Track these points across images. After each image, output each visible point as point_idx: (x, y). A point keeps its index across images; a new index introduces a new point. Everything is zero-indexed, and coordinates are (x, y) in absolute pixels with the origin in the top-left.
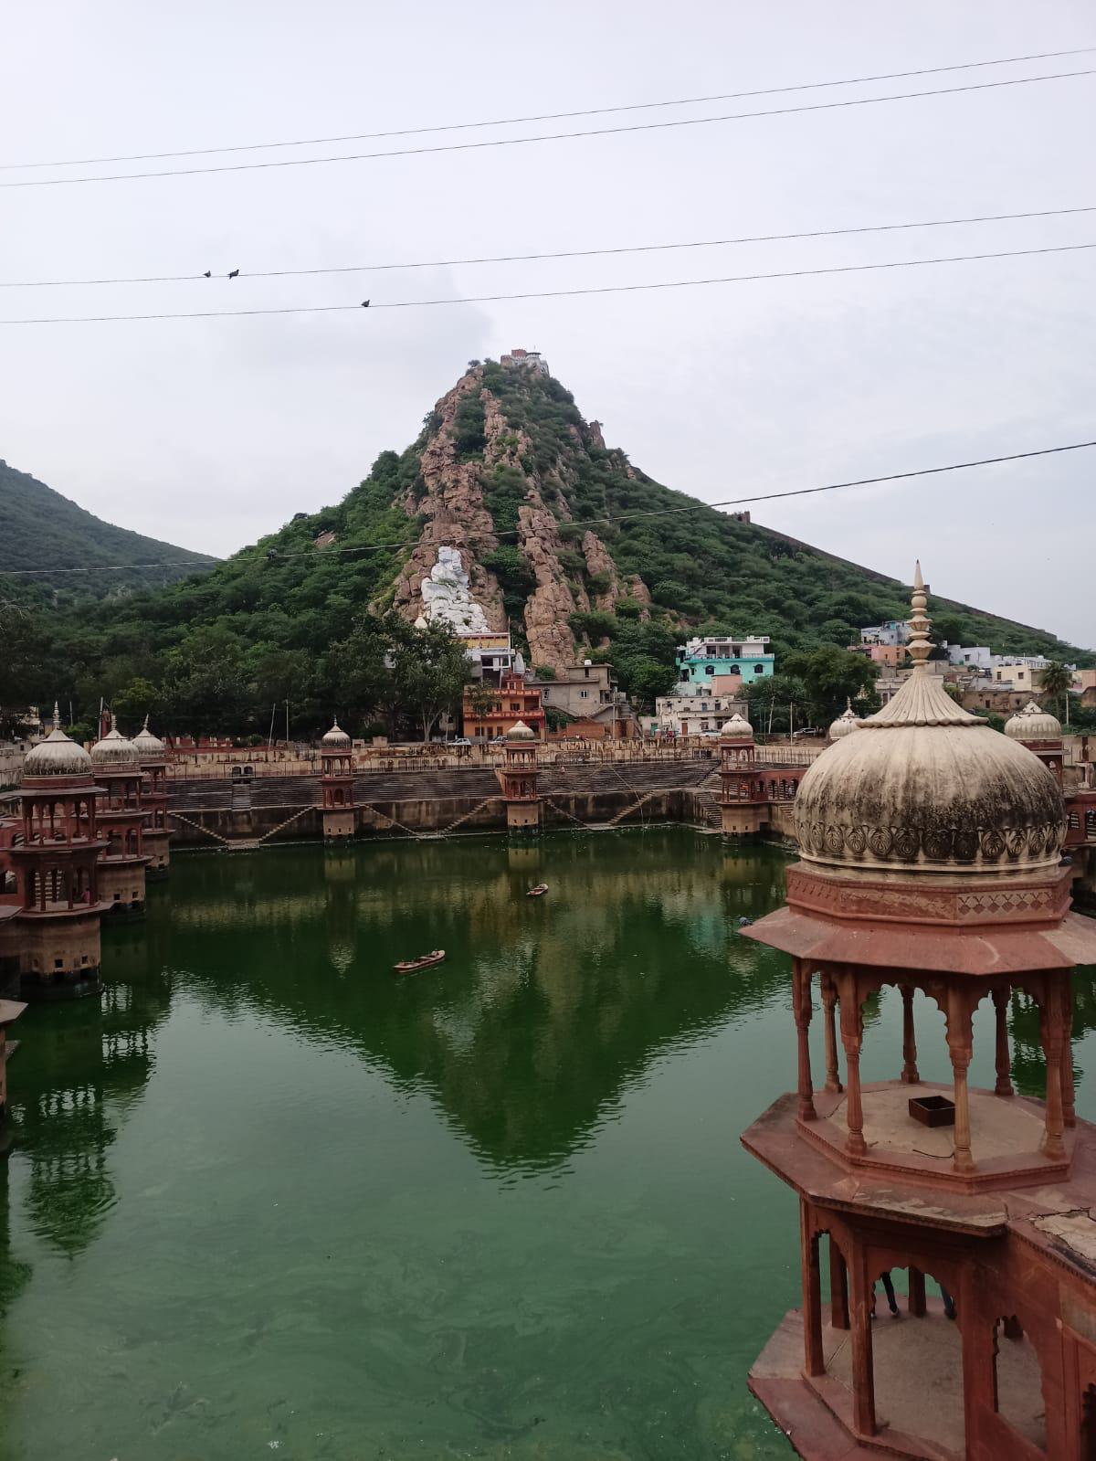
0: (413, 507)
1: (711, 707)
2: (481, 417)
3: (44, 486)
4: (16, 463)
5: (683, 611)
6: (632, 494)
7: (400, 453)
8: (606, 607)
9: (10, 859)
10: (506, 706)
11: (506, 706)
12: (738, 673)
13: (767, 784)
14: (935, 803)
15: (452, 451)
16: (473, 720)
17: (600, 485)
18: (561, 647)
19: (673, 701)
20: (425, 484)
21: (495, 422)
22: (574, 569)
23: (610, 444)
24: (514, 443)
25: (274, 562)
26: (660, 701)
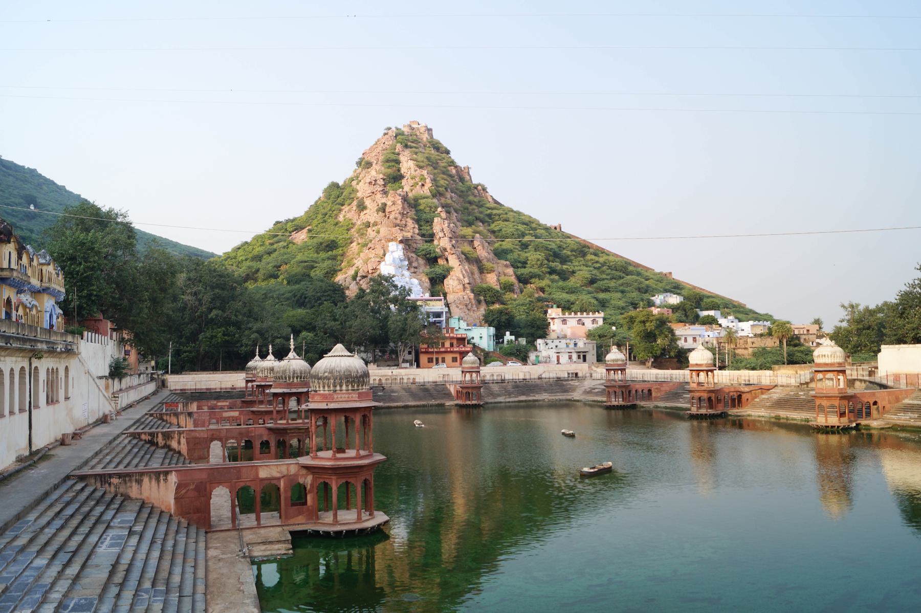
0: (356, 217)
1: (572, 346)
2: (398, 162)
3: (53, 183)
4: (6, 157)
6: (495, 212)
7: (341, 183)
8: (492, 280)
9: (267, 432)
10: (447, 344)
11: (447, 344)
12: (583, 324)
13: (633, 392)
15: (382, 182)
16: (426, 352)
17: (466, 201)
18: (469, 307)
19: (548, 341)
20: (364, 203)
21: (407, 165)
22: (468, 258)
23: (475, 181)
24: (441, 194)
25: (39, 185)
26: (539, 341)
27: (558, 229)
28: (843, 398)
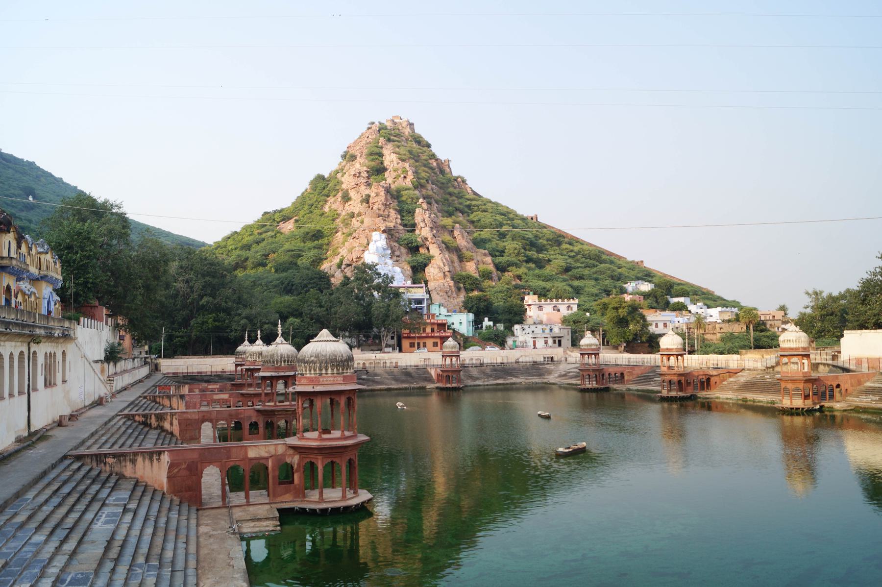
0: (341, 208)
1: (548, 331)
2: (381, 155)
3: (51, 175)
4: (6, 150)
5: (770, 383)
6: (474, 203)
7: (326, 176)
8: (471, 268)
9: (256, 413)
10: (428, 330)
11: (428, 330)
12: (559, 310)
13: (607, 375)
14: (510, 361)
15: (366, 175)
16: (408, 338)
17: (447, 193)
18: (449, 294)
19: (525, 327)
20: (348, 194)
21: (390, 158)
22: (448, 247)
23: (455, 173)
24: (423, 186)
25: (38, 177)
26: (516, 327)
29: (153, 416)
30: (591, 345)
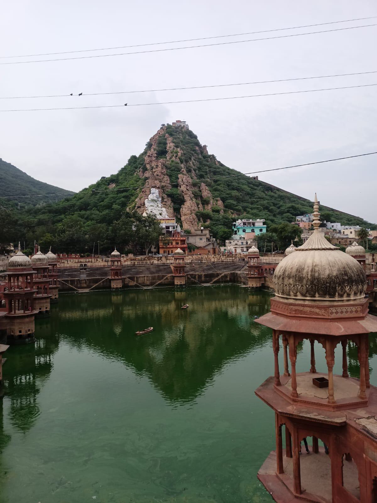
0: (142, 174)
1: (245, 243)
2: (165, 144)
3: (15, 167)
4: (5, 159)
5: (235, 210)
6: (218, 170)
7: (138, 156)
8: (208, 209)
9: (4, 296)
10: (174, 243)
11: (174, 243)
12: (254, 232)
13: (264, 270)
15: (156, 155)
16: (163, 248)
17: (206, 167)
18: (193, 223)
19: (232, 241)
20: (146, 166)
21: (170, 145)
22: (197, 196)
23: (210, 153)
24: (177, 152)
25: (94, 194)
26: (227, 241)
27: (256, 179)
28: (50, 212)
29: (136, 277)
30: (255, 252)
